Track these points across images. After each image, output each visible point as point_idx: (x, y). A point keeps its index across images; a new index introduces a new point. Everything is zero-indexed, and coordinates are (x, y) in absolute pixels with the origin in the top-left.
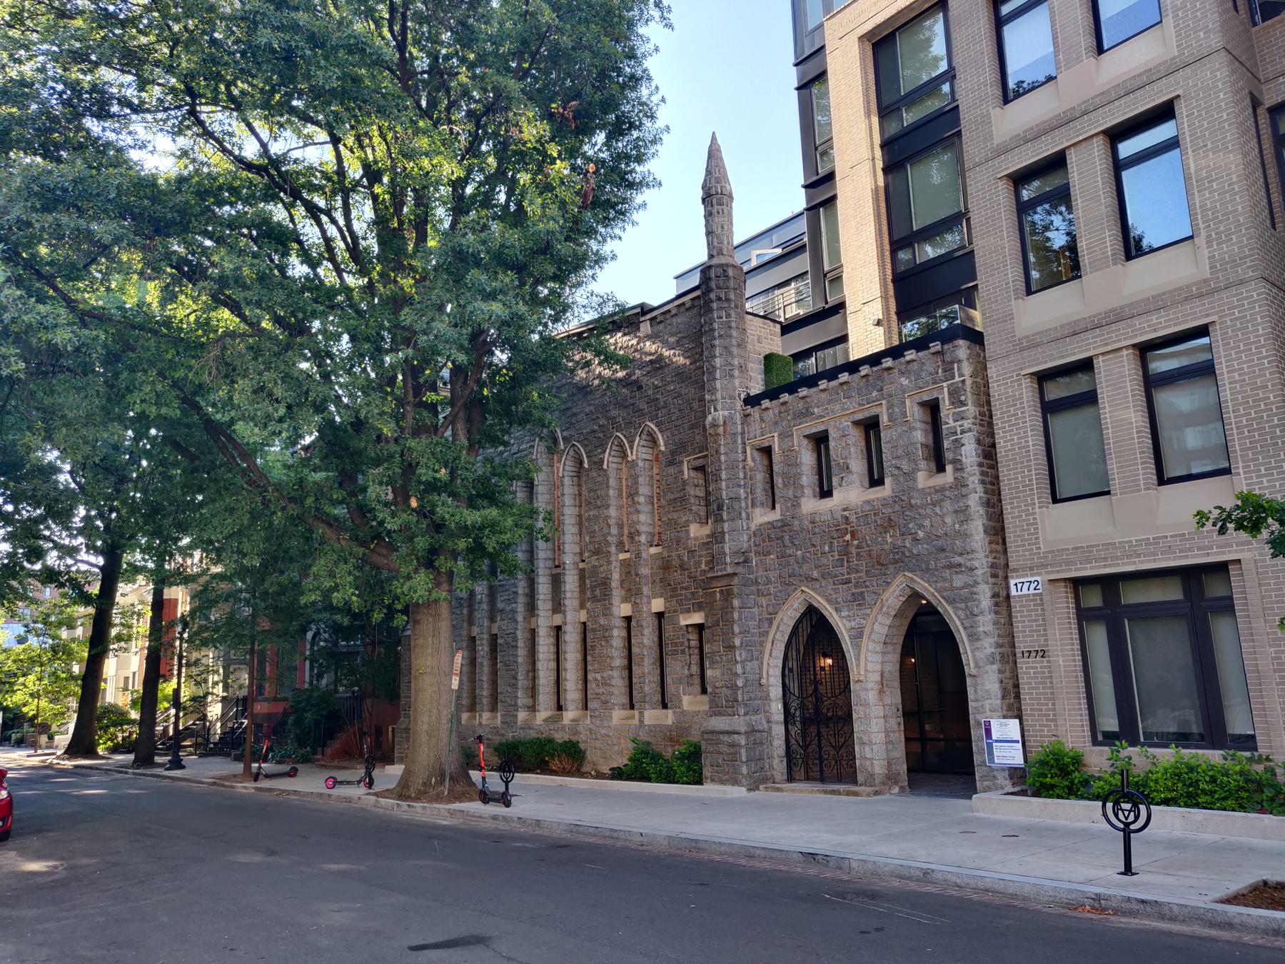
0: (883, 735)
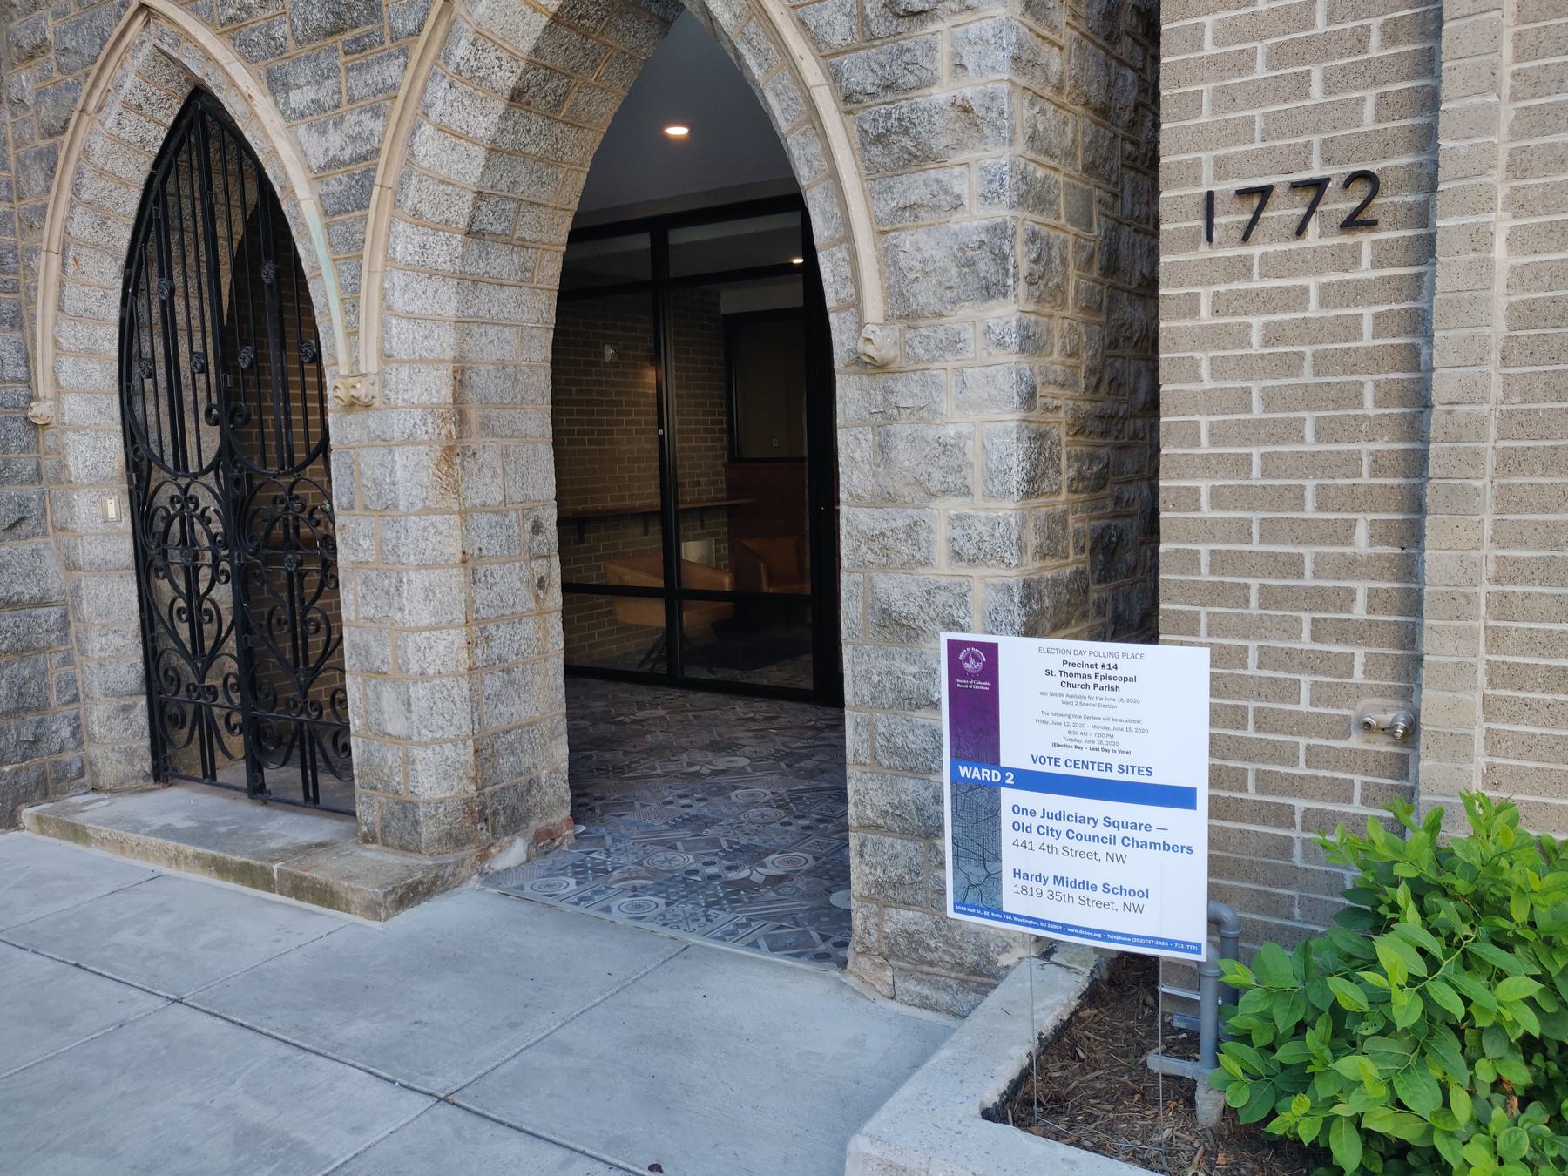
0: (458, 637)
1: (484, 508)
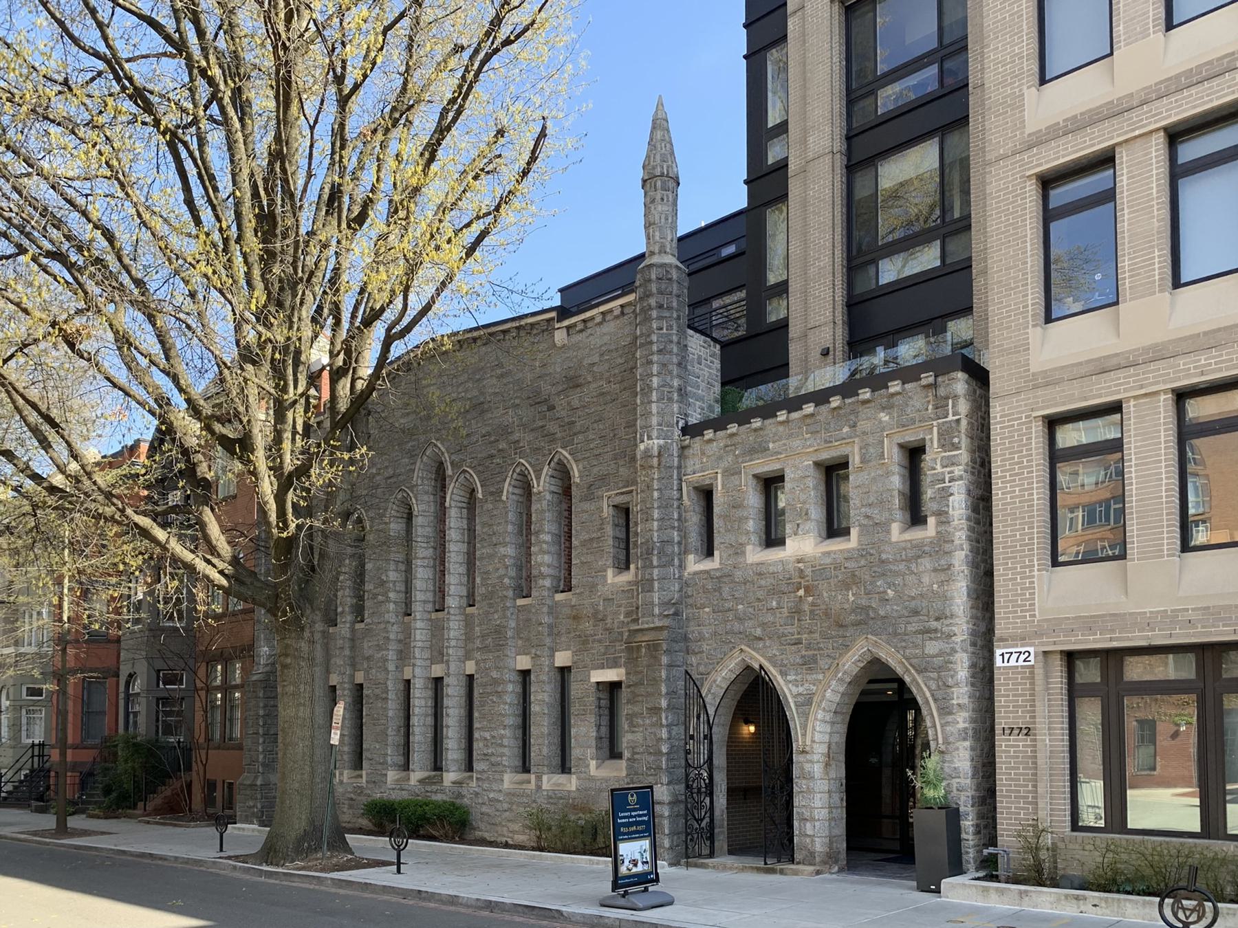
0: (826, 811)
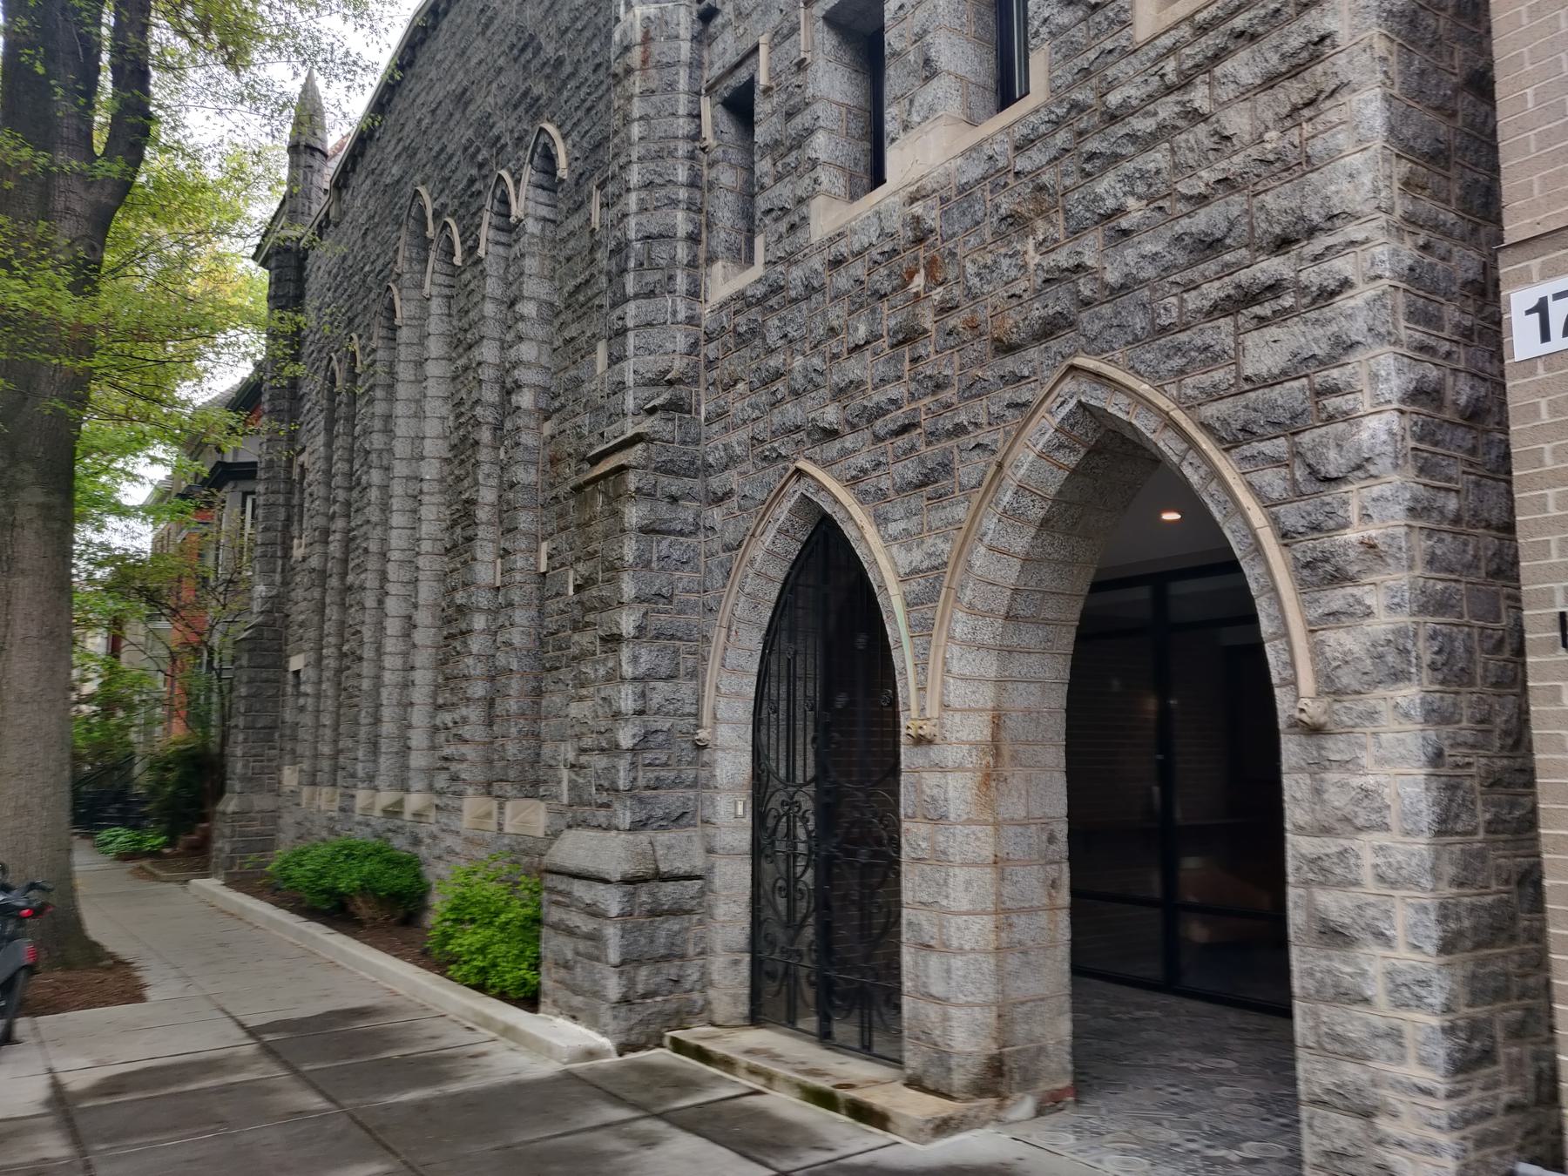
0: (988, 922)
1: (1013, 822)
